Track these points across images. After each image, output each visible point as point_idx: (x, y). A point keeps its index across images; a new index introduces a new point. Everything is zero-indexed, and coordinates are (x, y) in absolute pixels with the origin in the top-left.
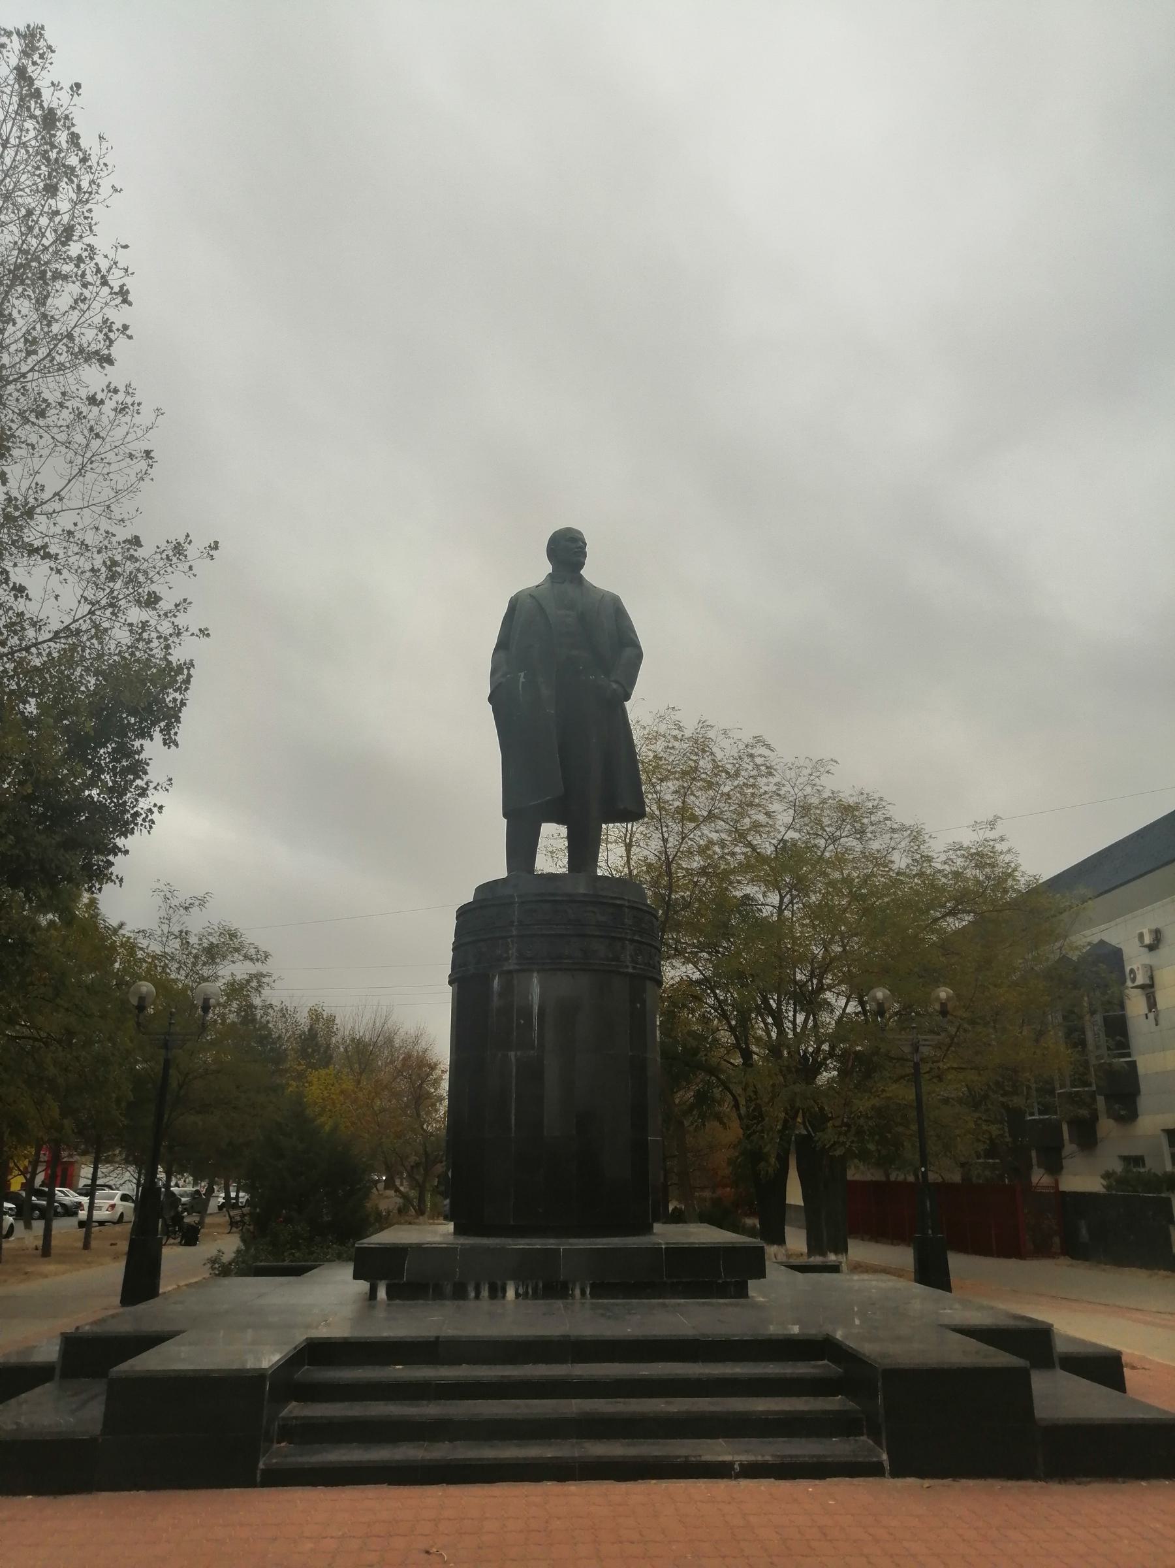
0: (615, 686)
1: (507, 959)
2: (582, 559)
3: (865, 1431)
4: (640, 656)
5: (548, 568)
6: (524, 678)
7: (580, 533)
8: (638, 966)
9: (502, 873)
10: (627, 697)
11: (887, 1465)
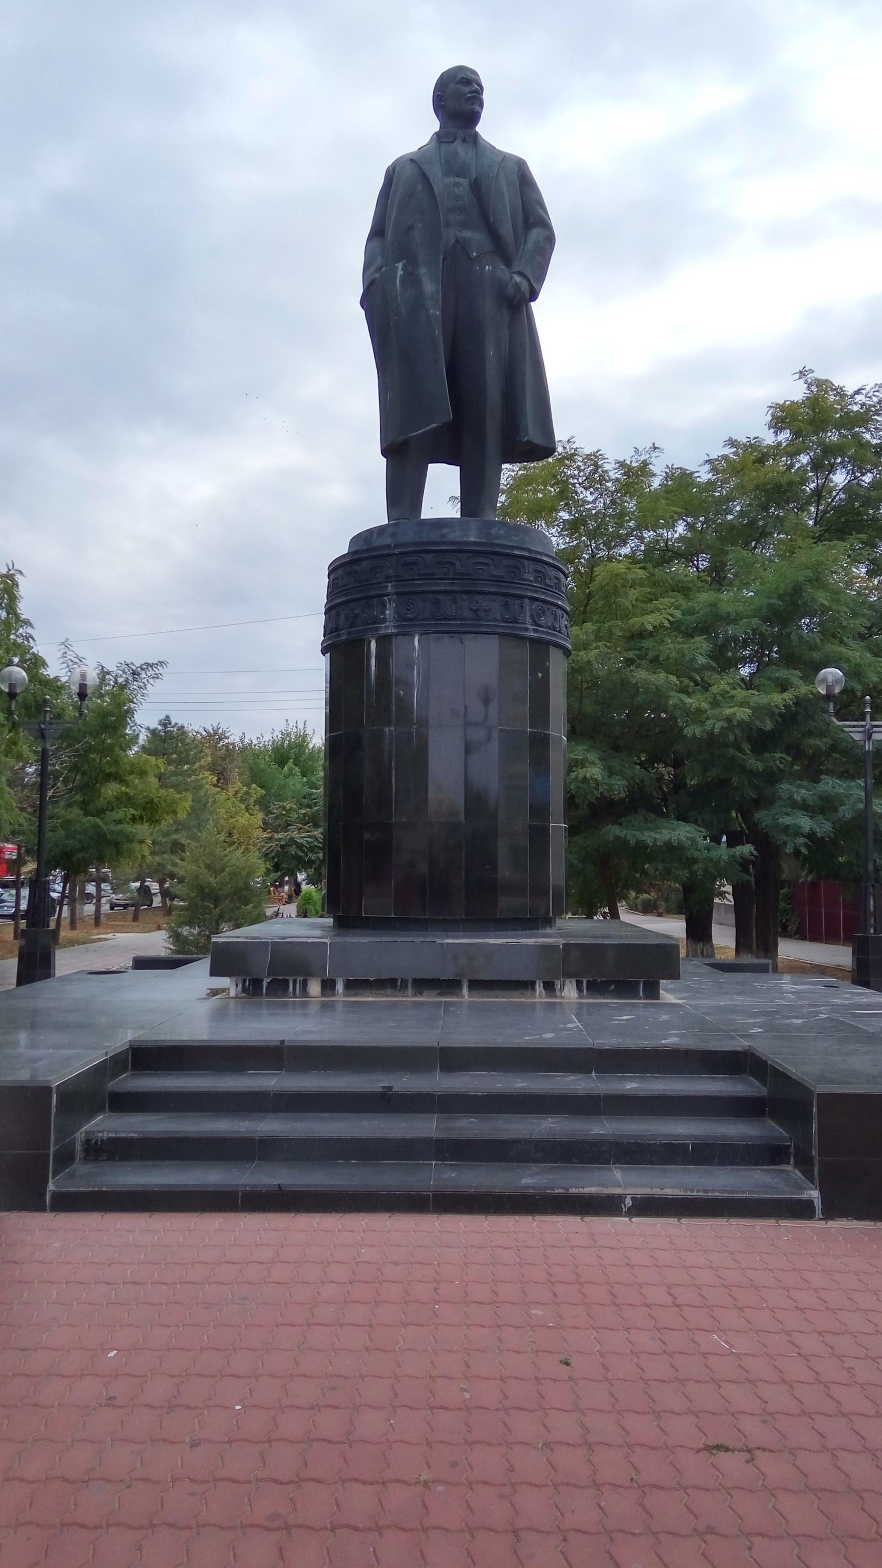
0: (518, 279)
1: (384, 621)
2: (477, 108)
3: (792, 1160)
4: (550, 240)
5: (435, 125)
6: (402, 269)
7: (474, 73)
8: (541, 629)
9: (382, 519)
10: (534, 295)
11: (818, 1204)
